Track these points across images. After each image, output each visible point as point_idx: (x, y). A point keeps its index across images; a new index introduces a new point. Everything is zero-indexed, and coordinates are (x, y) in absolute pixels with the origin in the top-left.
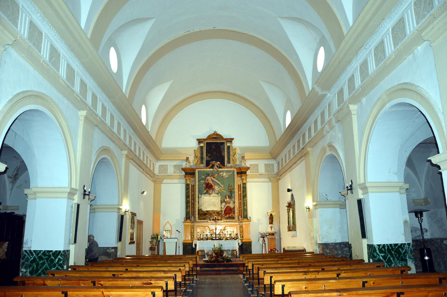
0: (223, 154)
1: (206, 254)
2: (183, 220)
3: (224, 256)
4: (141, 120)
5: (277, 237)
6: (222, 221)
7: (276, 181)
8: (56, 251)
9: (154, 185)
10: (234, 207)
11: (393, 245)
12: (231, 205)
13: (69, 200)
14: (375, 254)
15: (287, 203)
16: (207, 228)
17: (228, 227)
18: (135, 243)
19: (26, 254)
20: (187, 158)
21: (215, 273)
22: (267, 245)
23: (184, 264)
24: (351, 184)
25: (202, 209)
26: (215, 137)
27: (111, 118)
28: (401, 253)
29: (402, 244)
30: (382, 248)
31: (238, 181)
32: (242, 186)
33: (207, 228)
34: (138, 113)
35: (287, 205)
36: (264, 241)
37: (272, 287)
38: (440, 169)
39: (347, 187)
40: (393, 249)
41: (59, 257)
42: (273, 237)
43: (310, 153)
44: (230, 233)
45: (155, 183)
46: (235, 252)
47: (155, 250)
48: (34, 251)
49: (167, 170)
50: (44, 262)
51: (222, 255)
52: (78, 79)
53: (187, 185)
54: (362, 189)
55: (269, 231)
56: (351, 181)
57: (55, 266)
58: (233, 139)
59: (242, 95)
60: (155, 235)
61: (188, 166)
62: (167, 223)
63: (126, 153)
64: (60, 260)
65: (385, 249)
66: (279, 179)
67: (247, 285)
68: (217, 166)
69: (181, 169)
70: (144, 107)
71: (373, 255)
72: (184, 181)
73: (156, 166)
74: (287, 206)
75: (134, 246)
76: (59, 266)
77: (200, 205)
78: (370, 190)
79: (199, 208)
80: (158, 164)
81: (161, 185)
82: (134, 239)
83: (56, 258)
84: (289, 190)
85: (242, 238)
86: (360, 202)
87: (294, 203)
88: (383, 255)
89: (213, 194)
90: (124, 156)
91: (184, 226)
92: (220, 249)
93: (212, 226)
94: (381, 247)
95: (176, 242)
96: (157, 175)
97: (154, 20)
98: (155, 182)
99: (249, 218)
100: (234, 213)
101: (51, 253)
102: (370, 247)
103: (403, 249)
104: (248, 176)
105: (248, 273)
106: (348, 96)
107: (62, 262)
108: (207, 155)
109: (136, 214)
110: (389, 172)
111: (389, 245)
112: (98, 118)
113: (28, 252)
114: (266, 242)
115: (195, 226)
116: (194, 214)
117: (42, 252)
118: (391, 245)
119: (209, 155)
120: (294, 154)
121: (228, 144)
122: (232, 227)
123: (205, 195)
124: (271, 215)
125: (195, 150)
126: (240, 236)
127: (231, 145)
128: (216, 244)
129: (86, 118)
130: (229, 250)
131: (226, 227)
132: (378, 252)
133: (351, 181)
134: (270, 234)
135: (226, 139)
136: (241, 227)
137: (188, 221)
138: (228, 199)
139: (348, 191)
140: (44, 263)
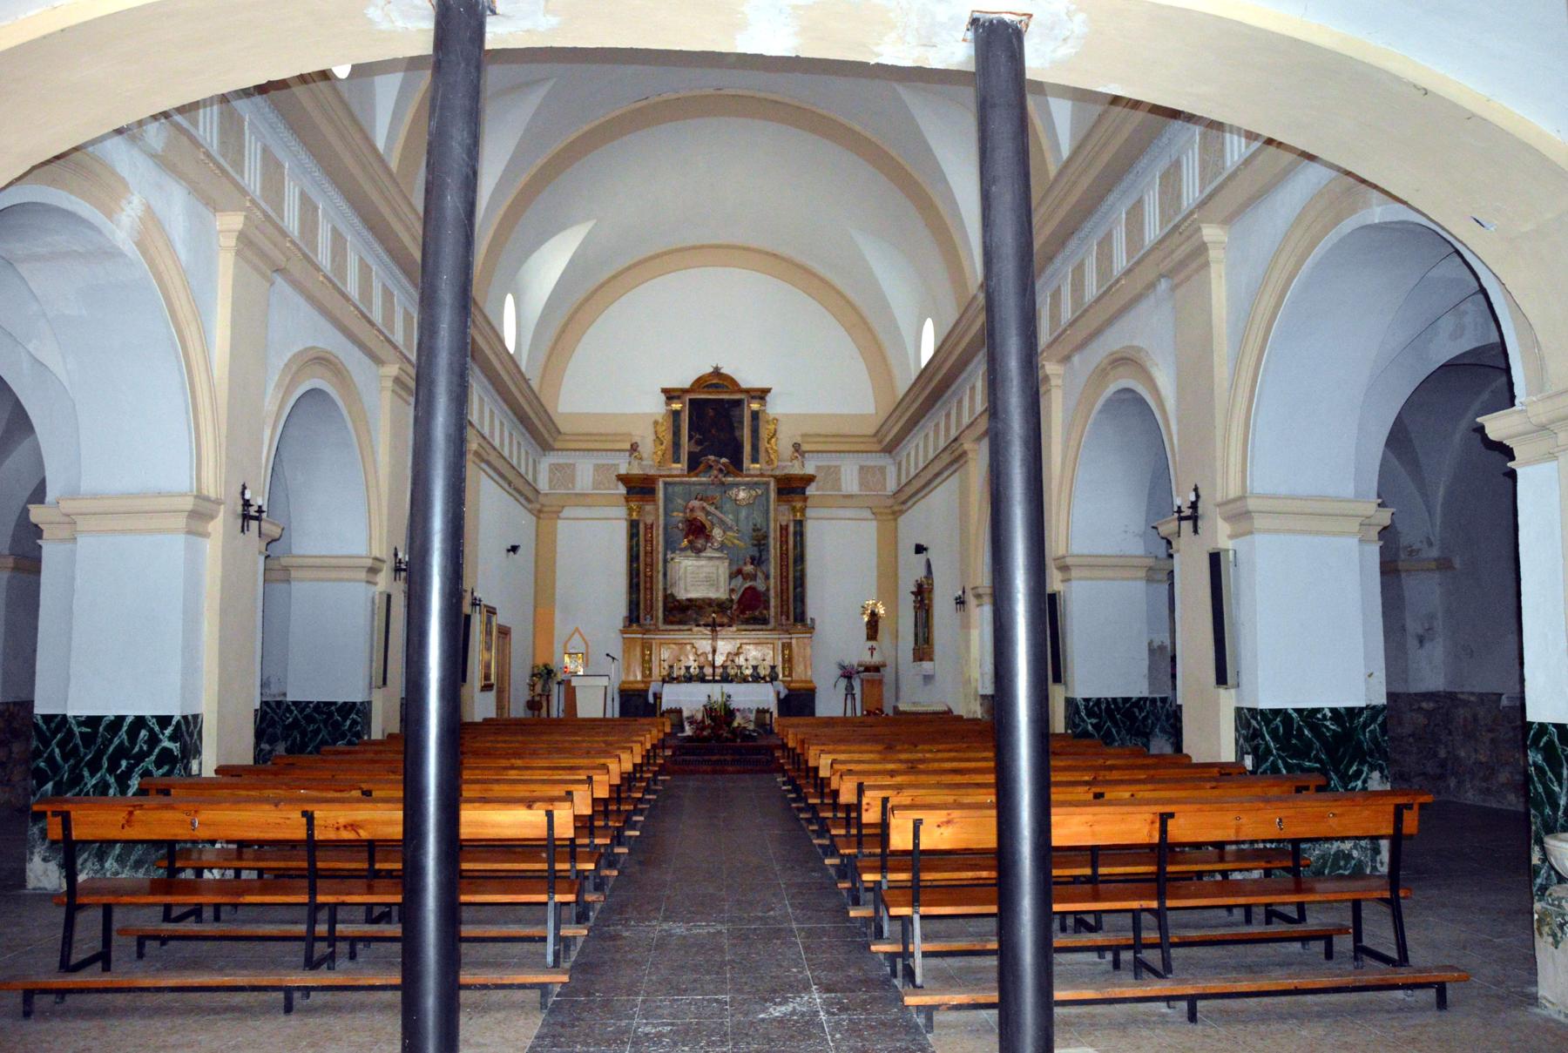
0: (737, 434)
1: (688, 718)
2: (620, 626)
3: (735, 724)
4: (501, 341)
5: (888, 674)
6: (734, 628)
7: (890, 517)
8: (345, 703)
9: (537, 523)
10: (768, 590)
11: (1120, 701)
12: (760, 585)
13: (189, 536)
14: (1077, 720)
15: (914, 582)
16: (689, 647)
17: (748, 647)
18: (495, 687)
19: (268, 710)
20: (632, 445)
21: (709, 768)
22: (858, 697)
23: (590, 773)
24: (1193, 498)
25: (676, 594)
26: (714, 382)
27: (405, 319)
28: (1137, 718)
29: (1140, 699)
30: (1093, 706)
31: (780, 515)
32: (791, 529)
33: (689, 647)
34: (537, 392)
35: (914, 589)
36: (850, 690)
37: (883, 830)
38: (1513, 458)
39: (1179, 507)
40: (1118, 709)
41: (353, 716)
42: (875, 675)
43: (970, 456)
44: (754, 663)
45: (538, 518)
46: (768, 716)
47: (540, 709)
48: (295, 703)
49: (573, 479)
50: (319, 727)
51: (731, 722)
53: (633, 527)
54: (1228, 519)
55: (867, 658)
56: (1196, 490)
57: (343, 736)
58: (767, 391)
59: (800, 259)
60: (541, 666)
61: (636, 470)
62: (573, 634)
63: (240, 227)
64: (354, 722)
65: (1100, 709)
66: (902, 512)
67: (820, 845)
68: (721, 470)
69: (614, 477)
70: (509, 299)
71: (1074, 722)
72: (622, 512)
73: (542, 466)
74: (912, 593)
75: (492, 695)
76: (352, 736)
77: (669, 583)
78: (1259, 522)
79: (665, 589)
80: (546, 462)
81: (556, 525)
82: (493, 677)
83: (345, 720)
84: (920, 549)
85: (789, 679)
86: (1215, 559)
87: (932, 584)
88: (1094, 721)
89: (709, 550)
90: (389, 384)
91: (625, 644)
92: (725, 705)
93: (704, 642)
94: (1091, 704)
95: (606, 687)
96: (546, 495)
97: (551, 83)
98: (538, 513)
99: (809, 622)
100: (767, 608)
101: (333, 708)
102: (1070, 703)
103: (1141, 710)
104: (809, 500)
105: (812, 781)
107: (359, 728)
108: (690, 438)
109: (495, 609)
110: (1126, 532)
111: (1343, 711)
112: (288, 245)
113: (274, 705)
114: (857, 691)
115: (654, 641)
116: (651, 609)
117: (311, 705)
118: (1114, 700)
119: (698, 436)
120: (947, 435)
121: (755, 406)
122: (759, 648)
123: (683, 554)
124: (873, 614)
125: (656, 423)
126: (783, 673)
127: (763, 408)
128: (716, 691)
129: (244, 239)
130: (750, 711)
131: (744, 646)
132: (1083, 714)
133: (1196, 490)
134: (867, 669)
135: (747, 391)
136: (787, 646)
137: (635, 626)
138: (749, 568)
139: (1182, 522)
140: (317, 732)
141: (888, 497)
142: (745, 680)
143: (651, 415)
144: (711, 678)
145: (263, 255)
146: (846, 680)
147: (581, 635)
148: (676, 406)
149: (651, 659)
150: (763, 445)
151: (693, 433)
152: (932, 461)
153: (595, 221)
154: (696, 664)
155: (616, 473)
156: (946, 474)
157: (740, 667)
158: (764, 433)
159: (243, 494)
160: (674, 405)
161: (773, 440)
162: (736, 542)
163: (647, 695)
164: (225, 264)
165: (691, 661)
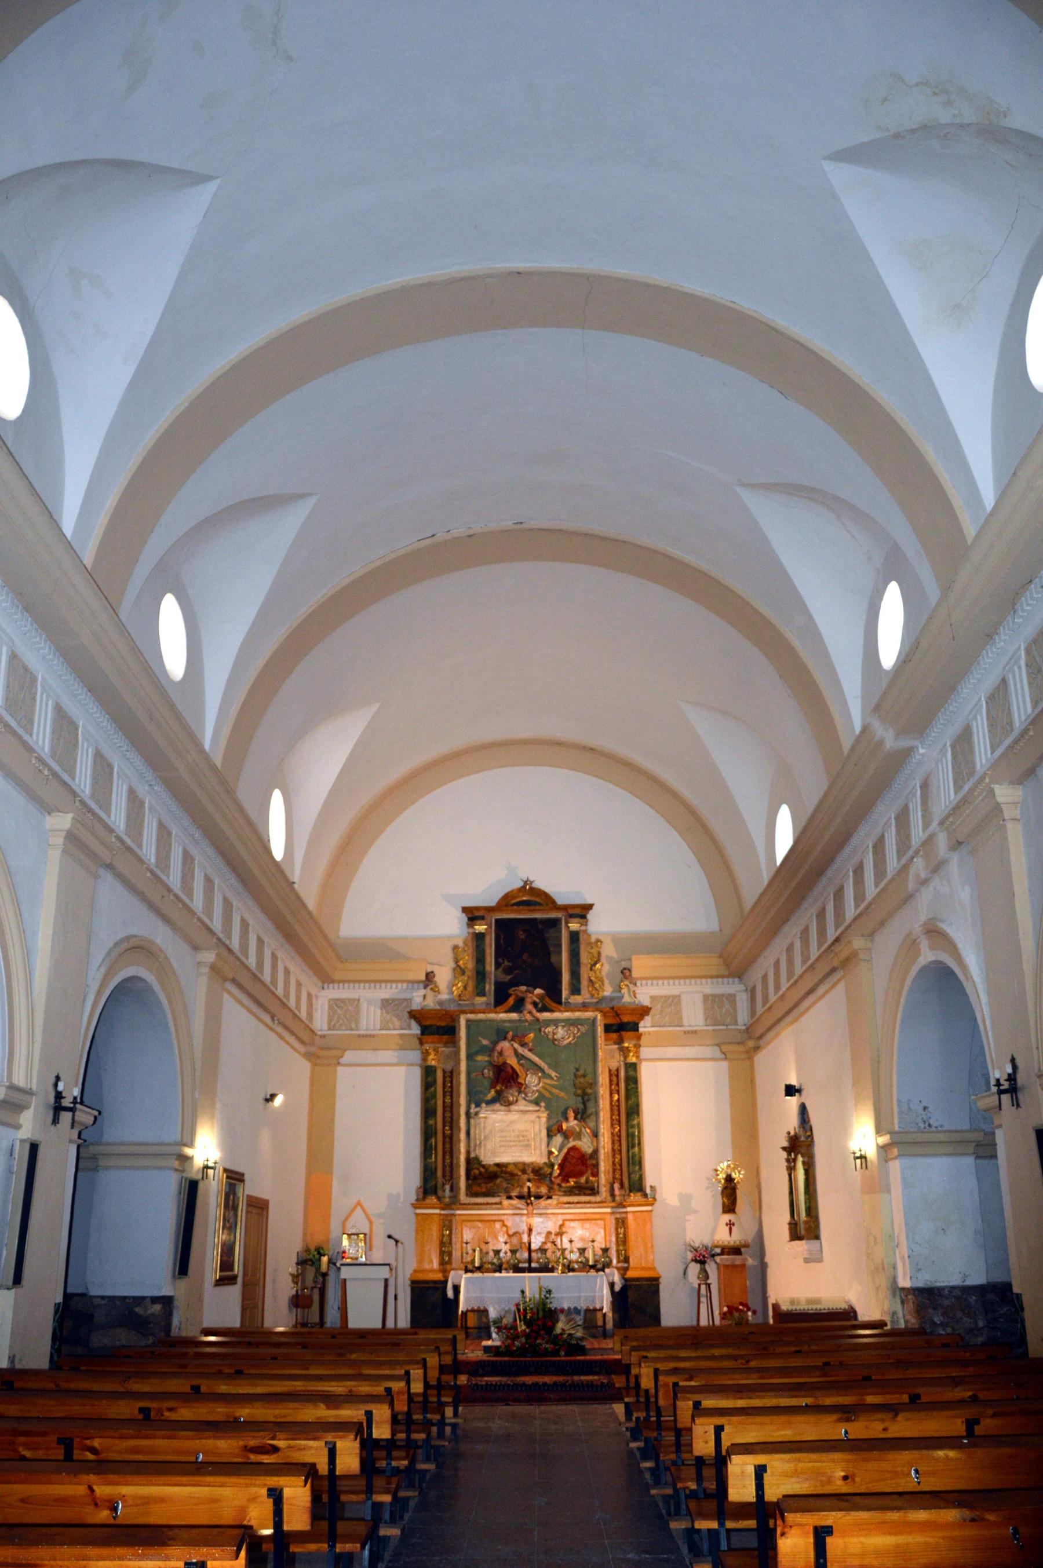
0: (554, 959)
1: (495, 1322)
2: (413, 1198)
10: (596, 1152)
12: (585, 1145)
16: (498, 1225)
17: (572, 1224)
18: (240, 1280)
22: (714, 1288)
25: (482, 1158)
32: (622, 1074)
33: (498, 1225)
35: (786, 1144)
39: (998, 1080)
42: (738, 1260)
44: (580, 1245)
46: (599, 1315)
47: (309, 1306)
51: (553, 1327)
52: (47, 705)
53: (428, 1073)
55: (723, 1236)
56: (1013, 1061)
58: (590, 907)
60: (313, 1249)
61: (431, 1003)
69: (406, 1015)
70: (277, 798)
72: (415, 1056)
74: (784, 1149)
79: (468, 1152)
82: (236, 1267)
87: (811, 1136)
89: (522, 1102)
92: (544, 1304)
95: (386, 1281)
96: (323, 1036)
99: (648, 1191)
100: (596, 1174)
104: (643, 1038)
106: (989, 755)
108: (498, 965)
109: (243, 1175)
114: (713, 1279)
116: (450, 1174)
119: (506, 963)
121: (574, 926)
122: (587, 1225)
124: (729, 1179)
125: (455, 948)
127: (583, 928)
128: (530, 1284)
129: (71, 837)
130: (577, 1311)
131: (567, 1223)
133: (1013, 1061)
135: (565, 908)
136: (621, 1223)
137: (432, 1200)
138: (573, 1123)
141: (740, 1031)
142: (569, 1268)
143: (449, 938)
144: (526, 1265)
145: (92, 854)
146: (698, 1265)
147: (364, 1211)
148: (481, 928)
149: (451, 1239)
150: (585, 973)
151: (500, 960)
152: (801, 976)
153: (377, 706)
154: (508, 1247)
155: (409, 1010)
156: (821, 990)
157: (563, 1250)
158: (585, 958)
159: (56, 1085)
160: (477, 927)
161: (598, 966)
162: (554, 1090)
163: (446, 1287)
164: (55, 856)
165: (501, 1243)
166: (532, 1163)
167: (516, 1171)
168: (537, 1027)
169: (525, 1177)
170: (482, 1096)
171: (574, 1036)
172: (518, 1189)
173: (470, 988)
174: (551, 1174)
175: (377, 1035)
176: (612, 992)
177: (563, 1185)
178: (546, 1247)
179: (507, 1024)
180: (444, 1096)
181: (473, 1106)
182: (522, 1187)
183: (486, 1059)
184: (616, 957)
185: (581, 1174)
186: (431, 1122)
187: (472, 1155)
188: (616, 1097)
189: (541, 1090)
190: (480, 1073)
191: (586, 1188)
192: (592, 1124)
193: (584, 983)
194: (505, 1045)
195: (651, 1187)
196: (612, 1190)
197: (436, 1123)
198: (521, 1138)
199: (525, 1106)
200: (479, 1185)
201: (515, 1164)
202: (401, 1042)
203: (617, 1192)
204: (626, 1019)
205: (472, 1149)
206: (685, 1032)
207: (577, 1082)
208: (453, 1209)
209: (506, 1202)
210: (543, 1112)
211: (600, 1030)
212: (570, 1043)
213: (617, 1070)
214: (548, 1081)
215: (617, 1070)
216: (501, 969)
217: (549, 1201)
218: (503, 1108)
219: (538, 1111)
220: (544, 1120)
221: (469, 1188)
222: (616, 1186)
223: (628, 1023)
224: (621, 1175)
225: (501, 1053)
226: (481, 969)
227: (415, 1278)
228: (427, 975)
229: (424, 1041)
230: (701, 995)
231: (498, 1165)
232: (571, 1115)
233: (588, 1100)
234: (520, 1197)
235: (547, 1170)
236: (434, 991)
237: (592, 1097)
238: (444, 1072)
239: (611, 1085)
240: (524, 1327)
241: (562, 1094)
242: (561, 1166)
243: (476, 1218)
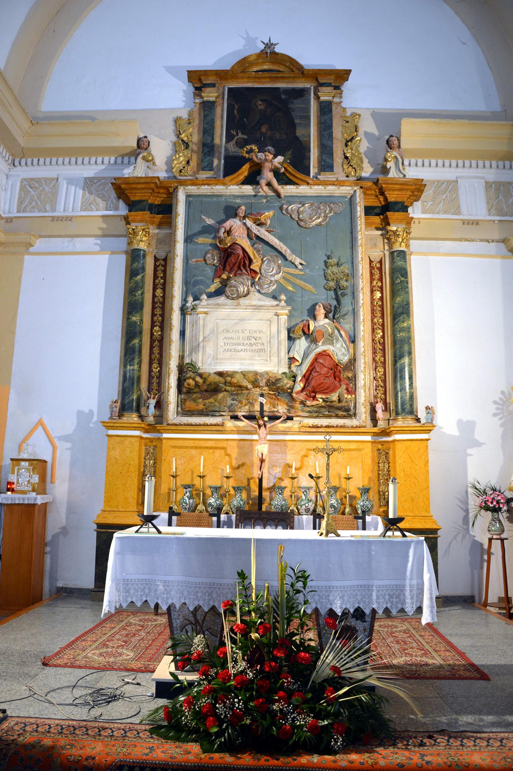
0: (300, 132)
79: (182, 358)
99: (422, 414)
100: (352, 391)
108: (229, 138)
119: (240, 135)
125: (177, 120)
151: (234, 132)
166: (267, 373)
167: (245, 383)
168: (277, 204)
169: (258, 391)
170: (202, 287)
171: (326, 217)
172: (247, 407)
173: (194, 163)
174: (292, 388)
175: (76, 217)
176: (372, 173)
177: (308, 403)
178: (283, 484)
179: (238, 201)
180: (154, 289)
181: (190, 299)
182: (252, 404)
183: (210, 241)
184: (377, 133)
185: (329, 390)
186: (135, 319)
187: (187, 360)
188: (378, 295)
189: (282, 281)
190: (202, 259)
191: (339, 409)
192: (347, 326)
193: (338, 159)
194: (235, 223)
195: (427, 408)
196: (373, 411)
197: (141, 321)
198: (253, 341)
199: (260, 300)
200: (194, 400)
201: (244, 374)
202: (104, 226)
203: (380, 414)
204: (392, 197)
205: (187, 353)
206: (464, 222)
207: (329, 271)
208: (159, 431)
209: (230, 424)
210: (283, 308)
211: (360, 211)
212: (320, 224)
213: (381, 262)
214: (292, 271)
215: (381, 262)
216: (234, 142)
217: (289, 424)
218: (229, 302)
219: (278, 305)
220: (284, 318)
221: (181, 403)
222: (379, 407)
223: (396, 203)
224: (385, 393)
225: (229, 232)
226: (209, 140)
227: (103, 521)
228: (139, 140)
229: (130, 218)
230: (484, 181)
231: (220, 374)
232: (321, 312)
233: (344, 295)
234: (250, 417)
235: (287, 383)
236: (148, 161)
237: (349, 291)
238: (156, 259)
239: (372, 280)
240: (242, 665)
241: (309, 287)
242: (307, 378)
243: (191, 444)
